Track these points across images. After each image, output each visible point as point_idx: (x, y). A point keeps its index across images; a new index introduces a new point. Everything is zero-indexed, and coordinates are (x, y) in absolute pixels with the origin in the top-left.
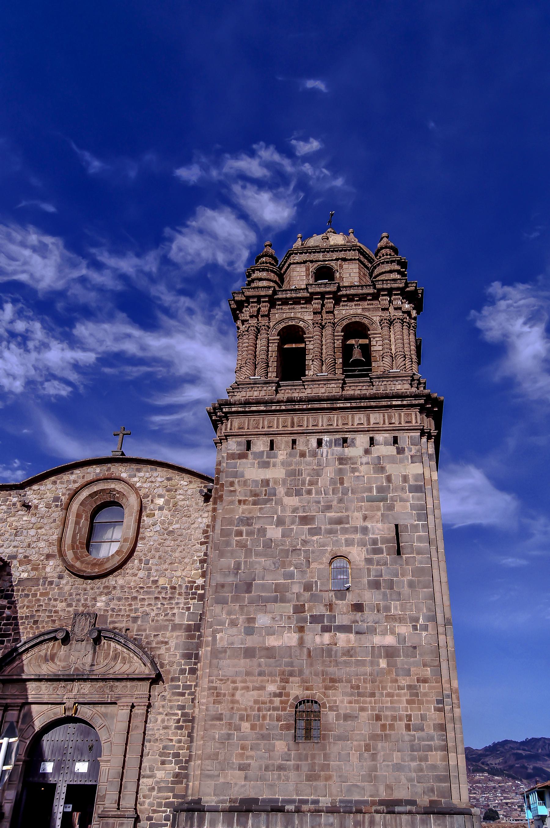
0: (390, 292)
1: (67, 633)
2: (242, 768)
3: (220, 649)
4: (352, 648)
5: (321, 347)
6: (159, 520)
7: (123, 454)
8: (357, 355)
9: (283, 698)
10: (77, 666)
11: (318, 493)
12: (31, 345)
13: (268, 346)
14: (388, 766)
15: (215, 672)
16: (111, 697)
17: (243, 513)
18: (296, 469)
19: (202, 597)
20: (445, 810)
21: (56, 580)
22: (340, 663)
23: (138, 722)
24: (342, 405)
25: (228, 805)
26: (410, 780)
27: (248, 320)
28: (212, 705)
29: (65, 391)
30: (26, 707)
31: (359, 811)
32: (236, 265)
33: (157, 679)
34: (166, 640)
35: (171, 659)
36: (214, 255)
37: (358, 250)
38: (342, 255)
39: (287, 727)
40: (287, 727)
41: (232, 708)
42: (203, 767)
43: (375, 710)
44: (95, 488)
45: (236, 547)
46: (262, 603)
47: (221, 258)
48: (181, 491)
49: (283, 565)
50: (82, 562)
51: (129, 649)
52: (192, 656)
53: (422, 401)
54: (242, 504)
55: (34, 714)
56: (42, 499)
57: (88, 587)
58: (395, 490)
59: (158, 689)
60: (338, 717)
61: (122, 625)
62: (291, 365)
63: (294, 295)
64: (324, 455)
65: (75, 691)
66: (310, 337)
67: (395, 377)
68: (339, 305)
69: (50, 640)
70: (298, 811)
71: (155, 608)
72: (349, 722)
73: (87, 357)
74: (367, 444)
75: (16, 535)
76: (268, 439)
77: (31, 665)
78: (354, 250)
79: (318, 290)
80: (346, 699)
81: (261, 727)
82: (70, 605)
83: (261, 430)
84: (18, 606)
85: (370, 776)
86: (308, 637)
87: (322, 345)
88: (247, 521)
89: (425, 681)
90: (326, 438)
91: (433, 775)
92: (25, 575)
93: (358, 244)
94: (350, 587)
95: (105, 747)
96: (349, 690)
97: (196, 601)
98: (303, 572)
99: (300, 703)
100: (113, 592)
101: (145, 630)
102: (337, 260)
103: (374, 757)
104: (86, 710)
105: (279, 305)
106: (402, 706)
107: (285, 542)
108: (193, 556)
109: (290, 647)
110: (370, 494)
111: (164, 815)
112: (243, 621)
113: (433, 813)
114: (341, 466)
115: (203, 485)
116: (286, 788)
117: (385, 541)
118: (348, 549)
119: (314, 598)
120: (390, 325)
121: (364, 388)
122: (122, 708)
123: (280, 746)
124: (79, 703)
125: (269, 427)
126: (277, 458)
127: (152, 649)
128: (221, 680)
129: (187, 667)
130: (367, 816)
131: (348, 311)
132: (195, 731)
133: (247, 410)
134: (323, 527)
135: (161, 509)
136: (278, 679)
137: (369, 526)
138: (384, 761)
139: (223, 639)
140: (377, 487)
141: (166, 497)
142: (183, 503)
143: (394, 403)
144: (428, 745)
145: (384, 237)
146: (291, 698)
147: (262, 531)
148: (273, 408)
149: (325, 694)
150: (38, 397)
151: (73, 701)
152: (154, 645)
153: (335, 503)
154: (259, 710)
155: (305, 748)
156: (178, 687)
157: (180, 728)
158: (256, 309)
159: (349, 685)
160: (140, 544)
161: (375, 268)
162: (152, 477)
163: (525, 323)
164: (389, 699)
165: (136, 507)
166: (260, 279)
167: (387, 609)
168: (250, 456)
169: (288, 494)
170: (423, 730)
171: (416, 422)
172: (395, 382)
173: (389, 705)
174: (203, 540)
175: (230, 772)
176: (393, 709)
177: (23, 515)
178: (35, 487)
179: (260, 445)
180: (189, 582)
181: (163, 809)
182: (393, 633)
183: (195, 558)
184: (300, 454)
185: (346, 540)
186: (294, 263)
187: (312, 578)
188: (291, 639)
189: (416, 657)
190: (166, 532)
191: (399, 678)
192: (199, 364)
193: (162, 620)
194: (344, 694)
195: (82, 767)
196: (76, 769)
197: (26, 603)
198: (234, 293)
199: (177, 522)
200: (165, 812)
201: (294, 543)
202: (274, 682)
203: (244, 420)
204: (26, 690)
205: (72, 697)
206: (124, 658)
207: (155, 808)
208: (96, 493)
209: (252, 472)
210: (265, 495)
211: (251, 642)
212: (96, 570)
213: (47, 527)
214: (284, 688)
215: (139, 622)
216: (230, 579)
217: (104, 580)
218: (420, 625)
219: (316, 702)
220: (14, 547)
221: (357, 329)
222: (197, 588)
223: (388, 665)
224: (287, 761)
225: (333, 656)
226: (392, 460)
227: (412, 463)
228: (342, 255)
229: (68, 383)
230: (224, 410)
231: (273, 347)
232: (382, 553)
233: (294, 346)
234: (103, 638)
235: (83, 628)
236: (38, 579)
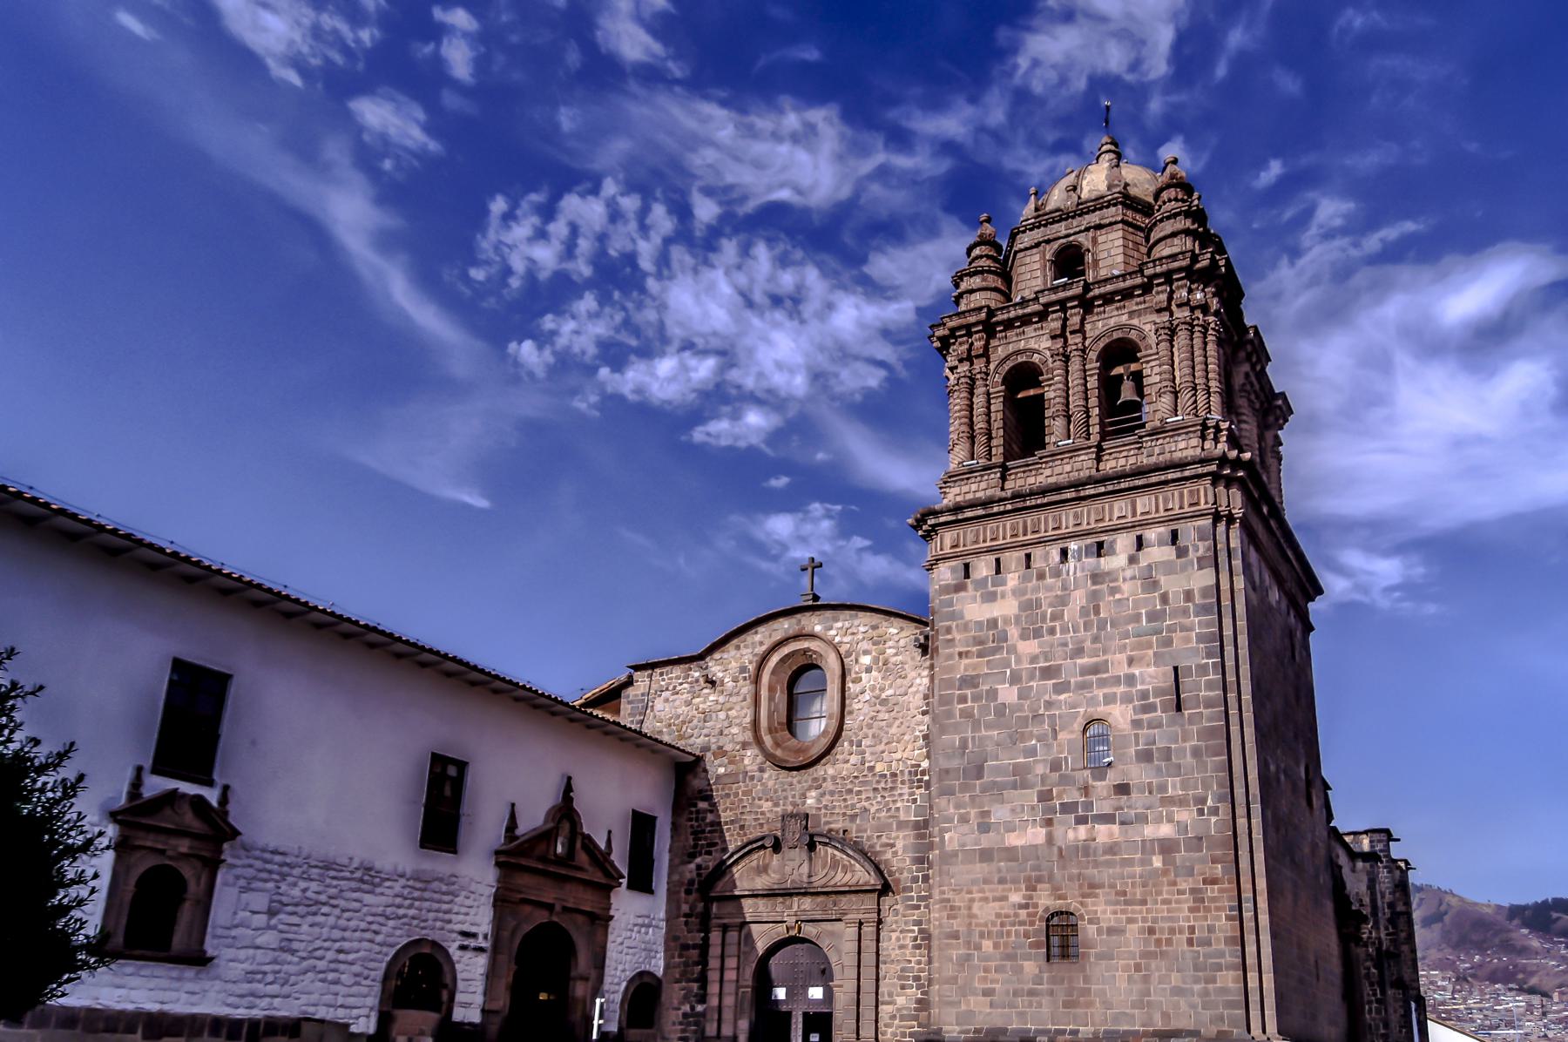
1: (776, 838)
2: (986, 993)
5: (1068, 391)
7: (816, 598)
11: (1065, 630)
12: (808, 309)
13: (991, 403)
21: (757, 774)
23: (869, 944)
24: (1092, 492)
26: (1193, 1006)
29: (875, 379)
32: (1145, 67)
33: (885, 889)
38: (1094, 218)
39: (1035, 945)
40: (1035, 945)
44: (786, 650)
46: (996, 791)
47: (1115, 59)
48: (890, 643)
49: (1023, 737)
50: (784, 749)
53: (1214, 468)
55: (755, 936)
58: (1173, 615)
59: (887, 901)
60: (1099, 931)
61: (838, 826)
63: (1020, 312)
65: (795, 908)
67: (1177, 430)
73: (899, 312)
76: (992, 558)
77: (744, 878)
80: (1109, 908)
82: (776, 805)
84: (720, 808)
86: (1058, 831)
88: (969, 681)
89: (1214, 881)
90: (1073, 546)
92: (722, 770)
95: (836, 969)
96: (1113, 897)
98: (1048, 746)
102: (1087, 229)
106: (1183, 915)
108: (914, 730)
116: (1038, 1016)
117: (1159, 692)
119: (1065, 780)
123: (1030, 967)
131: (1105, 323)
135: (869, 670)
137: (1137, 672)
146: (1040, 910)
147: (993, 694)
148: (996, 510)
150: (833, 398)
151: (794, 919)
152: (878, 848)
153: (1088, 644)
154: (1002, 925)
155: (1060, 967)
156: (911, 898)
157: (918, 947)
160: (847, 721)
165: (838, 671)
167: (1163, 788)
169: (1024, 636)
175: (972, 999)
176: (1171, 919)
178: (717, 656)
179: (983, 568)
182: (1170, 820)
185: (1105, 696)
188: (1037, 835)
194: (1108, 903)
195: (816, 993)
199: (891, 686)
202: (1017, 890)
208: (788, 656)
209: (974, 610)
211: (986, 841)
214: (1031, 898)
216: (955, 763)
221: (1121, 351)
222: (923, 773)
223: (1164, 863)
226: (1168, 568)
228: (1094, 218)
229: (881, 364)
231: (997, 405)
235: (794, 832)
236: (737, 774)
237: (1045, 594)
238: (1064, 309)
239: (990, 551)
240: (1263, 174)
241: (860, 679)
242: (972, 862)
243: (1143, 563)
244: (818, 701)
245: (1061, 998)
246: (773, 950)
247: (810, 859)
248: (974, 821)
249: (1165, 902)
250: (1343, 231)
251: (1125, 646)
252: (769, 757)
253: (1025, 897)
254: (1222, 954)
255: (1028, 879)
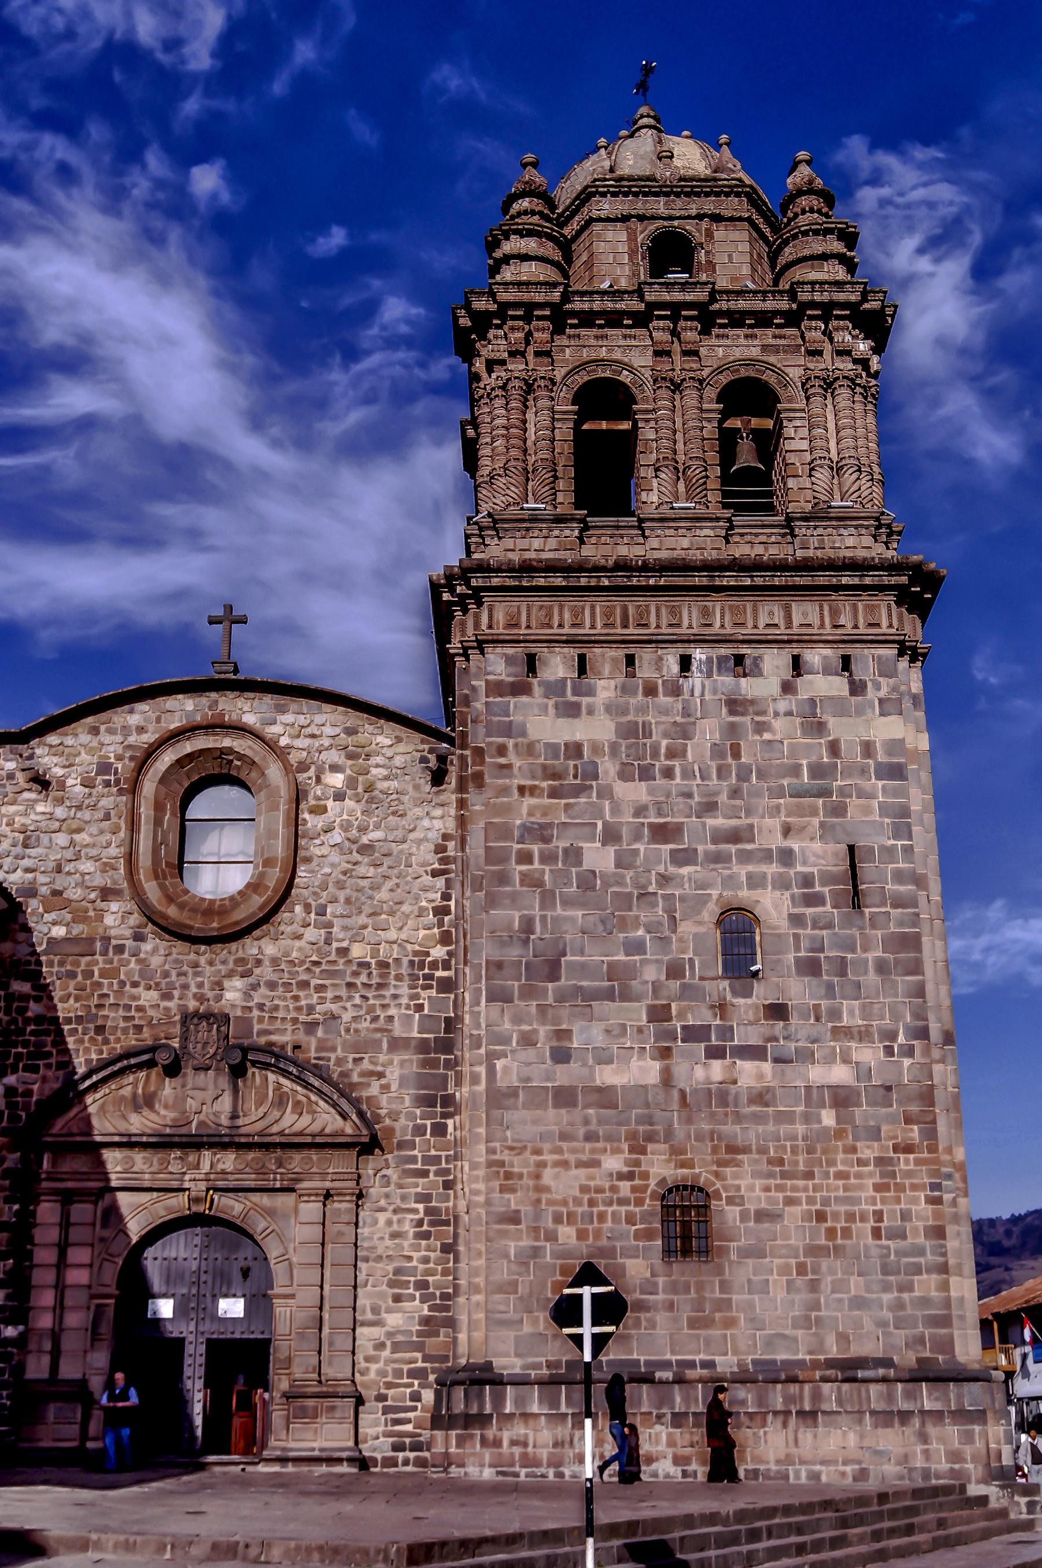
0: (827, 311)
3: (505, 1091)
4: (768, 1089)
5: (674, 432)
6: (338, 820)
8: (746, 456)
9: (637, 1182)
10: (202, 1117)
11: (688, 774)
13: (547, 426)
14: (840, 1300)
15: (499, 1134)
16: (282, 1180)
17: (530, 814)
18: (637, 723)
19: (447, 986)
20: (946, 1375)
21: (129, 943)
22: (745, 1116)
25: (545, 1371)
26: (883, 1324)
27: (503, 362)
28: (497, 1195)
30: (108, 1197)
31: (794, 1380)
32: (186, 50)
33: (370, 1145)
34: (380, 1068)
35: (394, 1106)
36: (129, 15)
37: (747, 195)
38: (709, 205)
41: (539, 1201)
42: (490, 1307)
43: (814, 1203)
45: (522, 885)
48: (379, 760)
49: (623, 924)
50: (182, 906)
51: (307, 1086)
52: (438, 1101)
53: (904, 580)
54: (527, 793)
55: (124, 1210)
56: (71, 765)
57: (202, 960)
58: (847, 773)
59: (370, 1165)
60: (744, 1216)
61: (284, 1038)
62: (603, 476)
63: (610, 305)
64: (697, 693)
65: (206, 1167)
66: (647, 411)
67: (843, 519)
68: (709, 334)
69: (140, 1066)
70: (680, 1380)
71: (348, 1005)
72: (766, 1225)
74: (787, 674)
75: (26, 846)
77: (106, 1113)
78: (738, 195)
79: (666, 297)
80: (758, 1183)
81: (598, 1234)
82: (167, 996)
83: (556, 631)
84: (57, 995)
85: (808, 1318)
87: (675, 432)
88: (541, 833)
89: (909, 1149)
90: (699, 655)
91: (923, 1316)
92: (59, 932)
93: (742, 175)
94: (758, 971)
96: (764, 1167)
97: (433, 993)
99: (670, 1191)
100: (257, 971)
101: (334, 1049)
102: (700, 217)
103: (814, 1286)
104: (231, 1202)
105: (572, 326)
106: (866, 1196)
107: (623, 877)
108: (417, 898)
109: (645, 1087)
110: (795, 781)
111: (408, 1390)
112: (546, 1037)
113: (927, 1380)
114: (732, 719)
115: (426, 747)
117: (828, 879)
118: (755, 895)
119: (688, 992)
120: (826, 390)
121: (773, 539)
122: (306, 1198)
124: (216, 1190)
125: (574, 625)
126: (594, 695)
127: (353, 1086)
128: (511, 1148)
129: (428, 1123)
130: (807, 1387)
131: (730, 350)
132: (461, 1240)
133: (525, 583)
134: (700, 848)
135: (339, 797)
136: (625, 1147)
138: (833, 1292)
139: (509, 1069)
140: (810, 767)
141: (348, 772)
142: (386, 784)
143: (844, 581)
144: (914, 1264)
145: (801, 162)
146: (652, 1183)
147: (574, 855)
148: (583, 582)
149: (717, 1175)
151: (203, 1186)
152: (355, 1078)
153: (723, 798)
154: (592, 1203)
155: (684, 1270)
156: (413, 1160)
157: (426, 1236)
158: (520, 335)
159: (765, 1158)
160: (302, 871)
161: (786, 243)
162: (313, 726)
163: (921, 251)
164: (841, 1183)
166: (525, 258)
167: (835, 1014)
168: (537, 690)
169: (624, 775)
170: (904, 1237)
171: (891, 626)
172: (842, 531)
173: (841, 1193)
174: (436, 866)
177: (36, 801)
178: (52, 739)
179: (557, 666)
180: (416, 953)
181: (406, 1380)
182: (846, 1060)
183: (424, 904)
184: (644, 688)
185: (750, 876)
186: (600, 220)
187: (683, 953)
188: (646, 1071)
189: (891, 1106)
190: (355, 847)
191: (859, 1144)
192: (87, 320)
193: (368, 1029)
194: (756, 1175)
195: (232, 1307)
196: (220, 1313)
197: (71, 989)
198: (472, 292)
199: (377, 827)
200: (411, 1385)
201: (643, 881)
202: (616, 1151)
203: (521, 605)
204: (102, 1164)
205: (202, 1176)
206: (297, 1104)
207: (389, 1379)
208: (190, 757)
209: (542, 724)
210: (575, 777)
211: (563, 1075)
212: (215, 925)
213: (94, 829)
214: (637, 1163)
215: (320, 1033)
216: (514, 953)
217: (234, 946)
218: (900, 1046)
219: (701, 1190)
220: (27, 870)
221: (749, 396)
222: (434, 966)
223: (839, 1121)
224: (651, 1294)
225: (731, 1104)
226: (840, 708)
227: (881, 715)
228: (709, 205)
230: (474, 583)
231: (565, 430)
232: (824, 904)
233: (604, 425)
234: (248, 1064)
236: (91, 940)
237: (659, 715)
238: (675, 318)
239: (571, 641)
240: (321, 240)
241: (324, 810)
242: (542, 1105)
243: (803, 695)
244: (216, 833)
245: (685, 1314)
246: (153, 1236)
247: (235, 1090)
248: (544, 1046)
249: (839, 1175)
250: (407, 342)
251: (778, 807)
252: (151, 916)
253: (627, 1163)
254: (921, 1252)
255: (632, 1136)
